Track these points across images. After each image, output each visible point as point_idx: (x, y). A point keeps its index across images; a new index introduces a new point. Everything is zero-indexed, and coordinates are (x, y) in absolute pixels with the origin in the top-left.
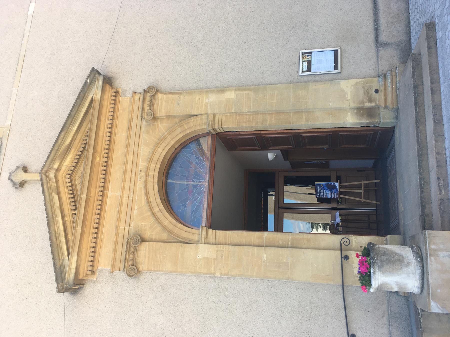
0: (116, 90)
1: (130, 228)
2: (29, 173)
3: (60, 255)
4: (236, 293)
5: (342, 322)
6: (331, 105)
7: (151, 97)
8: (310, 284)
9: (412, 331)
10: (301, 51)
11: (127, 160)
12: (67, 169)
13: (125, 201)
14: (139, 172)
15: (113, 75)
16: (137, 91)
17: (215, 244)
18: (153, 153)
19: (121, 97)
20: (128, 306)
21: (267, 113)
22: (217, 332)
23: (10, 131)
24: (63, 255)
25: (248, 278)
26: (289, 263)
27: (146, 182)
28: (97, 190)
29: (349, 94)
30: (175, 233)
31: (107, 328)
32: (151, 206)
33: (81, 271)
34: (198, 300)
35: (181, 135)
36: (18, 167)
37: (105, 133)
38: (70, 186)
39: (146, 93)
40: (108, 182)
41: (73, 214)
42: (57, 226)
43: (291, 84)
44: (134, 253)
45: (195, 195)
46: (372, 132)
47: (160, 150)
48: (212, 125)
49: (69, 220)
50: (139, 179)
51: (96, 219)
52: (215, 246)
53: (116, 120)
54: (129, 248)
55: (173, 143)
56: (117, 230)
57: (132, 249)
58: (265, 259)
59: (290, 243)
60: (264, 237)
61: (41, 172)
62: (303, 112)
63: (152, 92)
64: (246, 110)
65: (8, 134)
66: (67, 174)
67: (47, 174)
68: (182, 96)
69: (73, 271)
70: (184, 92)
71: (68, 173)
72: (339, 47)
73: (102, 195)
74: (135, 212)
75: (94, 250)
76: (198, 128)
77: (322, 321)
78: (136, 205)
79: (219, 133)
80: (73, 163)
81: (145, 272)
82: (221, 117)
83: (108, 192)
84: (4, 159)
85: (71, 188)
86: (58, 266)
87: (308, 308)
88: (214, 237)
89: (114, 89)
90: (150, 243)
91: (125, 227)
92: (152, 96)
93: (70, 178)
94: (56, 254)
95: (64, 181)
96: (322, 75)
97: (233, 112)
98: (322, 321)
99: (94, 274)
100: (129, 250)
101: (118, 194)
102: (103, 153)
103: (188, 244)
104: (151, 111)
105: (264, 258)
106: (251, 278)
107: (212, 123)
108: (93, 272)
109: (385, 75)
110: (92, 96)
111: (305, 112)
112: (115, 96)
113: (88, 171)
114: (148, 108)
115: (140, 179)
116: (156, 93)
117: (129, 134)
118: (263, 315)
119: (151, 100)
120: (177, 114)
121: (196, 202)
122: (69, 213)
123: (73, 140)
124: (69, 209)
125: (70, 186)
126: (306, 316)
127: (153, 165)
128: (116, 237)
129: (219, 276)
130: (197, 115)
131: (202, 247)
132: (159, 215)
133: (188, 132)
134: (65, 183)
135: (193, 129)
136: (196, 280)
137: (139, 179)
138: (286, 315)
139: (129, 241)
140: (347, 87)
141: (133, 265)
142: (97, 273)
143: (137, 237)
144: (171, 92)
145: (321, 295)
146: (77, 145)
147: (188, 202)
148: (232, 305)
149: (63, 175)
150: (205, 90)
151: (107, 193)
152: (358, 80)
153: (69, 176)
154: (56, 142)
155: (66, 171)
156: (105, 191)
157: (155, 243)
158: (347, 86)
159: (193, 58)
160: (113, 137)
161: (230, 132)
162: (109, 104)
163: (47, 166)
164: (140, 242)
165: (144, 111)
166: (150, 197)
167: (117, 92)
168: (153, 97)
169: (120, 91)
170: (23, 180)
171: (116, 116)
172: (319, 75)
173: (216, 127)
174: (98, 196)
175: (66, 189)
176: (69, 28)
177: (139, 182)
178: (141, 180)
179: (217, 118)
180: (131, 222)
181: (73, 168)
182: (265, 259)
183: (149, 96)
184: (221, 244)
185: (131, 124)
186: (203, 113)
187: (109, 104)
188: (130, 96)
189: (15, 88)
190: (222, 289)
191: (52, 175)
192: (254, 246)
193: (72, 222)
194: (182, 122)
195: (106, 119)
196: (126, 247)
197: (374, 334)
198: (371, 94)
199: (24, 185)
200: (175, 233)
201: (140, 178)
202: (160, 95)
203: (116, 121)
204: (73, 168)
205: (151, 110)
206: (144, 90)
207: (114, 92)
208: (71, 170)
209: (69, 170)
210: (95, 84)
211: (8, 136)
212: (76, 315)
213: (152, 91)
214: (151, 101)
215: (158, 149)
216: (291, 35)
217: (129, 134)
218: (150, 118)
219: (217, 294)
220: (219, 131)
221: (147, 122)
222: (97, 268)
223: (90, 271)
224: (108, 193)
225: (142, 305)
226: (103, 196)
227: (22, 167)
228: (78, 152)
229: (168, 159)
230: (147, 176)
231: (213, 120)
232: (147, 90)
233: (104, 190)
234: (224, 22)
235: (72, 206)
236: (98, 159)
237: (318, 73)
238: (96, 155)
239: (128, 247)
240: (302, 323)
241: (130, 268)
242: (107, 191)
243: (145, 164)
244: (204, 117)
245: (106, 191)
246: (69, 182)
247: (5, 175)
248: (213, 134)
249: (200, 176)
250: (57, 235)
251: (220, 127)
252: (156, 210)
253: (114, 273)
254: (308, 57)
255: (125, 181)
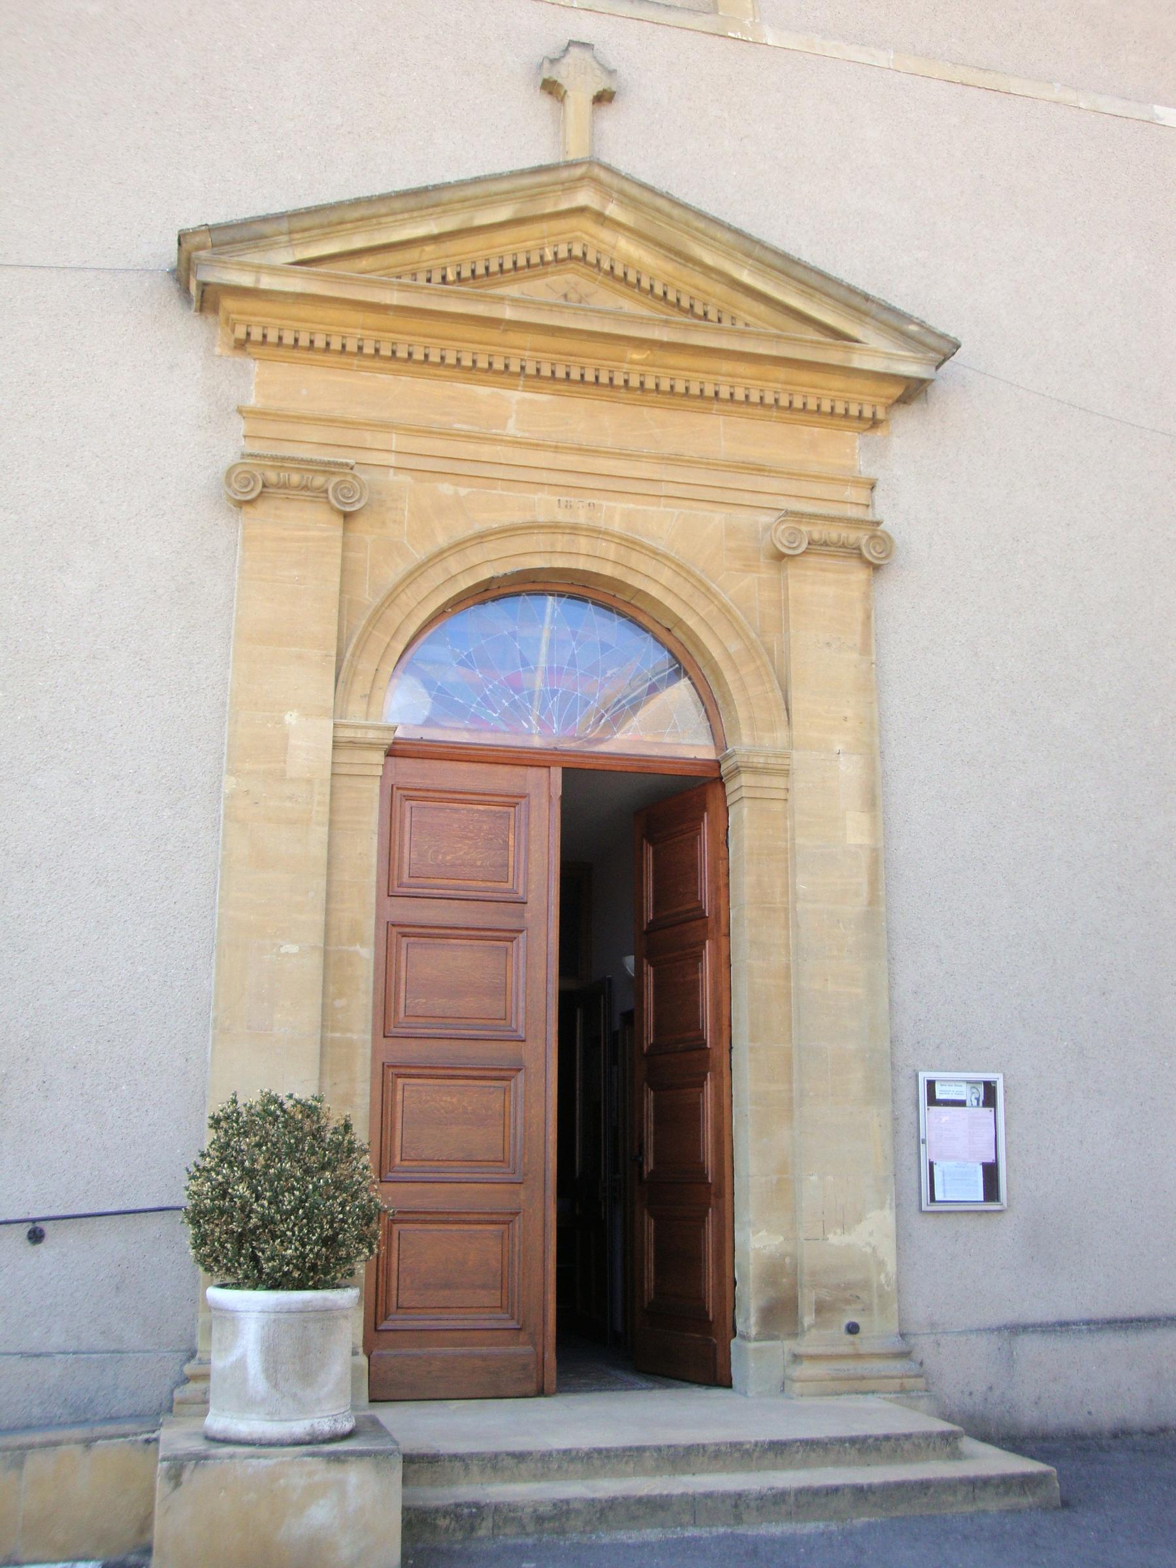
0: (882, 421)
1: (392, 470)
2: (593, 112)
3: (306, 234)
4: (169, 847)
5: (81, 1200)
6: (812, 1178)
7: (854, 543)
8: (202, 1098)
9: (59, 1425)
10: (1000, 1076)
11: (633, 458)
12: (603, 246)
13: (486, 451)
14: (588, 502)
15: (937, 406)
16: (878, 492)
17: (332, 774)
18: (654, 553)
19: (856, 434)
20: (128, 468)
21: (789, 961)
22: (40, 780)
23: (740, 42)
24: (307, 243)
25: (218, 888)
26: (271, 1030)
27: (553, 528)
28: (528, 353)
29: (847, 1239)
30: (374, 632)
31: (53, 397)
32: (469, 544)
33: (249, 305)
34: (145, 712)
35: (716, 653)
36: (611, 73)
37: (730, 379)
38: (542, 257)
39: (869, 527)
40: (555, 390)
41: (445, 269)
42: (406, 219)
43: (887, 1044)
44: (305, 488)
45: (504, 701)
46: (713, 1315)
47: (666, 575)
48: (751, 765)
49: (425, 257)
50: (563, 499)
51: (427, 352)
52: (328, 774)
53: (776, 417)
54: (324, 472)
55: (691, 622)
56: (385, 426)
57: (319, 480)
58: (283, 950)
59: (338, 1035)
60: (358, 947)
61: (592, 162)
62: (790, 1083)
63: (874, 548)
64: (802, 887)
65: (730, 34)
66: (584, 245)
67: (585, 182)
68: (855, 656)
69: (245, 280)
70: (872, 663)
71: (589, 248)
72: (1009, 1206)
73: (511, 372)
74: (446, 488)
75: (317, 348)
76: (742, 713)
77: (83, 1137)
78: (470, 490)
79: (723, 785)
80: (625, 265)
81: (238, 526)
82: (782, 795)
83: (520, 388)
84: (642, 20)
85: (535, 259)
86: (267, 229)
87: (124, 1090)
88: (356, 770)
89: (886, 411)
90: (339, 545)
91: (393, 454)
92: (859, 548)
93: (571, 257)
94: (307, 222)
95: (560, 237)
96: (915, 1150)
97: (794, 839)
98: (83, 1137)
99: (235, 348)
100: (315, 471)
101: (512, 429)
102: (660, 371)
103: (334, 679)
104: (804, 546)
105: (288, 946)
106: (217, 900)
107: (760, 766)
108: (241, 345)
109: (905, 1355)
110: (860, 337)
111: (791, 1090)
112: (860, 417)
113: (596, 326)
114: (816, 536)
115: (562, 505)
116: (869, 564)
117: (725, 466)
118: (97, 937)
119: (843, 546)
120: (792, 640)
121: (479, 704)
122: (447, 256)
123: (707, 270)
124: (463, 257)
125: (542, 257)
126: (98, 1085)
127: (610, 550)
128: (359, 423)
129: (226, 791)
130: (787, 710)
131: (324, 729)
132: (436, 575)
133: (729, 676)
134: (553, 239)
135: (736, 696)
136: (209, 707)
137: (563, 499)
138: (101, 1016)
139: (348, 471)
140: (871, 1234)
141: (264, 486)
142: (239, 359)
143: (359, 500)
144: (873, 618)
145: (165, 1136)
146: (687, 283)
147: (480, 676)
148: (128, 833)
149: (587, 233)
150: (877, 740)
151: (518, 386)
152: (891, 1267)
153: (577, 251)
154: (700, 215)
155: (595, 242)
156: (522, 378)
157: (339, 561)
158: (873, 1231)
159: (989, 695)
160: (716, 406)
161: (728, 827)
162: (833, 393)
163: (615, 182)
164: (343, 509)
165: (804, 520)
166: (499, 541)
167: (875, 423)
168: (855, 552)
169: (879, 433)
170: (566, 92)
171: (789, 419)
172: (915, 1139)
173: (745, 779)
174: (506, 358)
175: (532, 243)
176: (1104, 253)
177: (555, 499)
178: (559, 507)
179: (778, 782)
180: (414, 473)
181: (606, 266)
182: (283, 950)
183: (858, 539)
184: (332, 794)
185: (762, 473)
186: (795, 733)
187: (833, 393)
188: (862, 468)
189: (892, 57)
190: (179, 799)
191: (585, 197)
192: (328, 912)
193: (415, 266)
194: (766, 658)
195: (781, 383)
196: (326, 459)
197: (48, 1303)
198: (844, 1310)
199: (551, 93)
200: (371, 632)
201: (568, 506)
202: (860, 575)
203: (771, 417)
204: (606, 266)
205: (809, 544)
206: (878, 523)
207: (874, 414)
208: (598, 261)
209: (599, 255)
210: (902, 348)
211: (722, 36)
212: (98, 289)
213: (877, 547)
214: (840, 547)
215: (669, 567)
216: (1057, 1041)
217: (725, 466)
218: (781, 543)
219: (164, 781)
220: (730, 787)
221: (767, 528)
222: (256, 356)
223: (248, 334)
224: (514, 390)
225: (129, 519)
226: (506, 375)
227: (614, 89)
228: (664, 285)
229: (632, 602)
230: (574, 530)
231: (770, 766)
232: (879, 533)
233: (528, 376)
234: (1110, 809)
235: (473, 267)
236: (636, 356)
237: (922, 1137)
238: (650, 350)
239: (328, 468)
240: (75, 1067)
241: (254, 477)
242: (525, 386)
243: (617, 526)
244: (781, 735)
245: (522, 382)
246: (556, 254)
247: (586, 28)
248: (720, 767)
249: (741, 1519)
250: (374, 221)
251: (744, 792)
252: (454, 564)
253: (237, 418)
254: (976, 1099)
255: (556, 449)
